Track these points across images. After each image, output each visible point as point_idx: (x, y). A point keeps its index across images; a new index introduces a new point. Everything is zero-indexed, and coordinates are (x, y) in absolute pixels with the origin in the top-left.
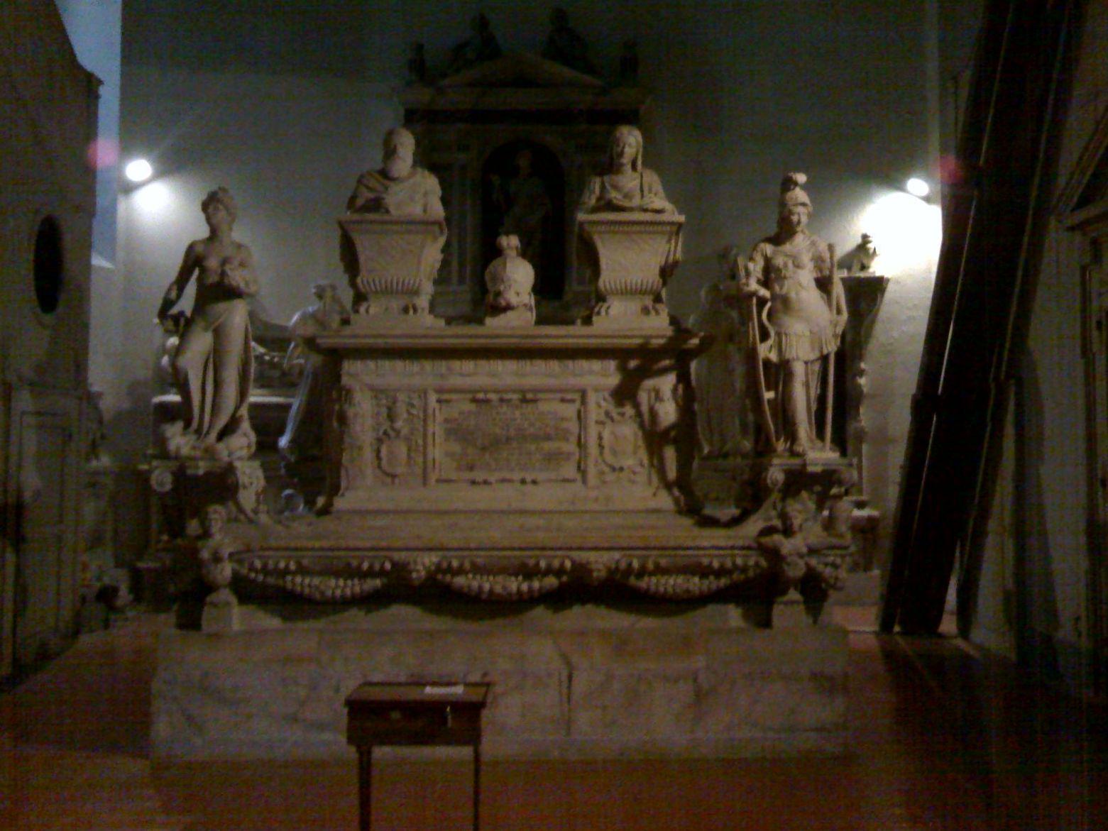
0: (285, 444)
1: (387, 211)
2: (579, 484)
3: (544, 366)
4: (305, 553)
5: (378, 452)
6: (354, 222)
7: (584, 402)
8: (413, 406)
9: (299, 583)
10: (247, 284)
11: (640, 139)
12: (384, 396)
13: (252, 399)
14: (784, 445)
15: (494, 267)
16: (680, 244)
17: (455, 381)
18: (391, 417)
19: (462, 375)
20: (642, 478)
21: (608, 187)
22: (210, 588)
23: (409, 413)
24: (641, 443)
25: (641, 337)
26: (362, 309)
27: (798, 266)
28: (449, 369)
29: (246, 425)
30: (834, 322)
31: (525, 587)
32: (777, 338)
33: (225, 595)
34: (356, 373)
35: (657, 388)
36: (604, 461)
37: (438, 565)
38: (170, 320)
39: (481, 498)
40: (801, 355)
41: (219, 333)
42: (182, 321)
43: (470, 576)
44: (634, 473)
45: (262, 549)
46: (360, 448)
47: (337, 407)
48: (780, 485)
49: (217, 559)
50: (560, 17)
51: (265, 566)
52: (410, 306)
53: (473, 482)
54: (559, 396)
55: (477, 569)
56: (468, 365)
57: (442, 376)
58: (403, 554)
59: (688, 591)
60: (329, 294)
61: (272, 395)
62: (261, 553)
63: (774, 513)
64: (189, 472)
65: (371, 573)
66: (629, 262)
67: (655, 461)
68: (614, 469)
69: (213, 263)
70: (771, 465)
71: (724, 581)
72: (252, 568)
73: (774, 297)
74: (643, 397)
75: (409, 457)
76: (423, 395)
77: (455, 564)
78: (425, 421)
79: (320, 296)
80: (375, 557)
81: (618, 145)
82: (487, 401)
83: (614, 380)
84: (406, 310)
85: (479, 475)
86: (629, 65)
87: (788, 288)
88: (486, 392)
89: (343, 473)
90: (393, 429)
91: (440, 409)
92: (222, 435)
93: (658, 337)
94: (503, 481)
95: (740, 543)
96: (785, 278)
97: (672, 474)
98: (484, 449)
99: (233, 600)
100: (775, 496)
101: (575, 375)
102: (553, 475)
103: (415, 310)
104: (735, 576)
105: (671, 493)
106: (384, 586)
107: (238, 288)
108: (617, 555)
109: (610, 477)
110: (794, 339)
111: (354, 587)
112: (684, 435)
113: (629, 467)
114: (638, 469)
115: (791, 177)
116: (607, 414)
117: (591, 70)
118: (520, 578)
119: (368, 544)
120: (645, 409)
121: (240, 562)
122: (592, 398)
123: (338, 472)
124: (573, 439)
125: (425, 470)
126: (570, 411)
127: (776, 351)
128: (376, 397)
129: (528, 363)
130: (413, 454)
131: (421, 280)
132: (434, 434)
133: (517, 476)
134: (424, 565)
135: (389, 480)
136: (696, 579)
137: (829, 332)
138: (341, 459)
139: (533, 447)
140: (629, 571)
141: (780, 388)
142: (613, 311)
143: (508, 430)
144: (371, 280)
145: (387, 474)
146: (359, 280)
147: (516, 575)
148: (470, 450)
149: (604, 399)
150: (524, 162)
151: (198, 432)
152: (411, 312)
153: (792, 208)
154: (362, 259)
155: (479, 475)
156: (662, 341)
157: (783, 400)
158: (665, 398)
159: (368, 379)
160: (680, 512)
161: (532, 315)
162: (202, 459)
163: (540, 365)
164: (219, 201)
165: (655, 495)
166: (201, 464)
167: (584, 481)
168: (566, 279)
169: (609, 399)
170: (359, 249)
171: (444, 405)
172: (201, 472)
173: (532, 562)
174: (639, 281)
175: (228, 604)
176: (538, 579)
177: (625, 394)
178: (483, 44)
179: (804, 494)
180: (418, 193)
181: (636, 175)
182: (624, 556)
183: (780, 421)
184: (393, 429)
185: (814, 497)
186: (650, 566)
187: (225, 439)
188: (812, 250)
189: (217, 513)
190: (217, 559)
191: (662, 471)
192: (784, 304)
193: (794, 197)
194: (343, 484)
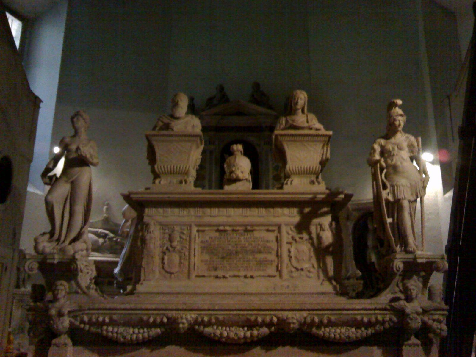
0: (117, 271)
1: (172, 129)
2: (278, 277)
4: (115, 312)
6: (154, 135)
7: (279, 231)
9: (110, 331)
10: (91, 156)
11: (306, 96)
14: (400, 249)
16: (329, 149)
17: (207, 220)
18: (171, 240)
22: (55, 334)
23: (181, 237)
24: (312, 254)
25: (310, 194)
27: (400, 148)
28: (203, 212)
31: (248, 334)
33: (65, 339)
34: (153, 215)
35: (321, 223)
36: (291, 264)
37: (196, 320)
39: (220, 285)
40: (406, 196)
41: (74, 185)
42: (54, 178)
43: (215, 327)
44: (309, 271)
45: (89, 309)
46: (152, 257)
47: (140, 234)
49: (60, 314)
50: (257, 86)
51: (90, 320)
53: (217, 277)
54: (266, 228)
55: (221, 323)
56: (215, 211)
57: (200, 217)
58: (174, 312)
59: (349, 337)
62: (88, 312)
63: (397, 289)
64: (49, 261)
65: (155, 325)
66: (303, 157)
67: (321, 265)
68: (297, 269)
70: (396, 259)
71: (370, 331)
72: (82, 322)
73: (388, 166)
74: (313, 229)
75: (181, 263)
76: (189, 228)
77: (206, 319)
78: (190, 242)
80: (158, 314)
82: (225, 231)
83: (297, 219)
84: (181, 182)
87: (396, 160)
88: (224, 226)
89: (142, 270)
90: (171, 246)
91: (199, 235)
93: (321, 194)
94: (234, 276)
95: (380, 306)
96: (393, 155)
97: (331, 273)
98: (223, 258)
99: (69, 341)
100: (398, 278)
101: (274, 216)
103: (186, 182)
104: (377, 328)
105: (331, 283)
106: (163, 333)
107: (86, 157)
108: (305, 314)
109: (295, 274)
110: (402, 188)
111: (144, 333)
112: (336, 250)
113: (306, 268)
114: (312, 270)
115: (394, 102)
116: (293, 238)
117: (270, 107)
118: (246, 329)
119: (154, 307)
120: (314, 235)
121: (75, 317)
122: (284, 229)
124: (274, 252)
126: (272, 236)
127: (392, 196)
129: (248, 209)
130: (182, 261)
131: (189, 167)
132: (195, 250)
133: (242, 273)
134: (186, 319)
135: (169, 275)
136: (353, 330)
139: (251, 257)
140: (312, 324)
143: (237, 247)
146: (156, 167)
147: (243, 327)
152: (184, 183)
153: (395, 117)
154: (158, 155)
155: (220, 273)
156: (323, 196)
157: (398, 223)
158: (326, 229)
159: (160, 219)
160: (337, 294)
161: (250, 185)
165: (322, 284)
167: (281, 276)
168: (269, 166)
170: (157, 150)
171: (200, 233)
172: (56, 261)
173: (253, 318)
175: (65, 344)
176: (256, 329)
177: (302, 227)
179: (415, 277)
182: (309, 314)
183: (397, 236)
184: (171, 246)
185: (421, 279)
186: (325, 321)
187: (73, 244)
188: (408, 140)
189: (63, 287)
190: (60, 314)
191: (325, 271)
194: (142, 277)
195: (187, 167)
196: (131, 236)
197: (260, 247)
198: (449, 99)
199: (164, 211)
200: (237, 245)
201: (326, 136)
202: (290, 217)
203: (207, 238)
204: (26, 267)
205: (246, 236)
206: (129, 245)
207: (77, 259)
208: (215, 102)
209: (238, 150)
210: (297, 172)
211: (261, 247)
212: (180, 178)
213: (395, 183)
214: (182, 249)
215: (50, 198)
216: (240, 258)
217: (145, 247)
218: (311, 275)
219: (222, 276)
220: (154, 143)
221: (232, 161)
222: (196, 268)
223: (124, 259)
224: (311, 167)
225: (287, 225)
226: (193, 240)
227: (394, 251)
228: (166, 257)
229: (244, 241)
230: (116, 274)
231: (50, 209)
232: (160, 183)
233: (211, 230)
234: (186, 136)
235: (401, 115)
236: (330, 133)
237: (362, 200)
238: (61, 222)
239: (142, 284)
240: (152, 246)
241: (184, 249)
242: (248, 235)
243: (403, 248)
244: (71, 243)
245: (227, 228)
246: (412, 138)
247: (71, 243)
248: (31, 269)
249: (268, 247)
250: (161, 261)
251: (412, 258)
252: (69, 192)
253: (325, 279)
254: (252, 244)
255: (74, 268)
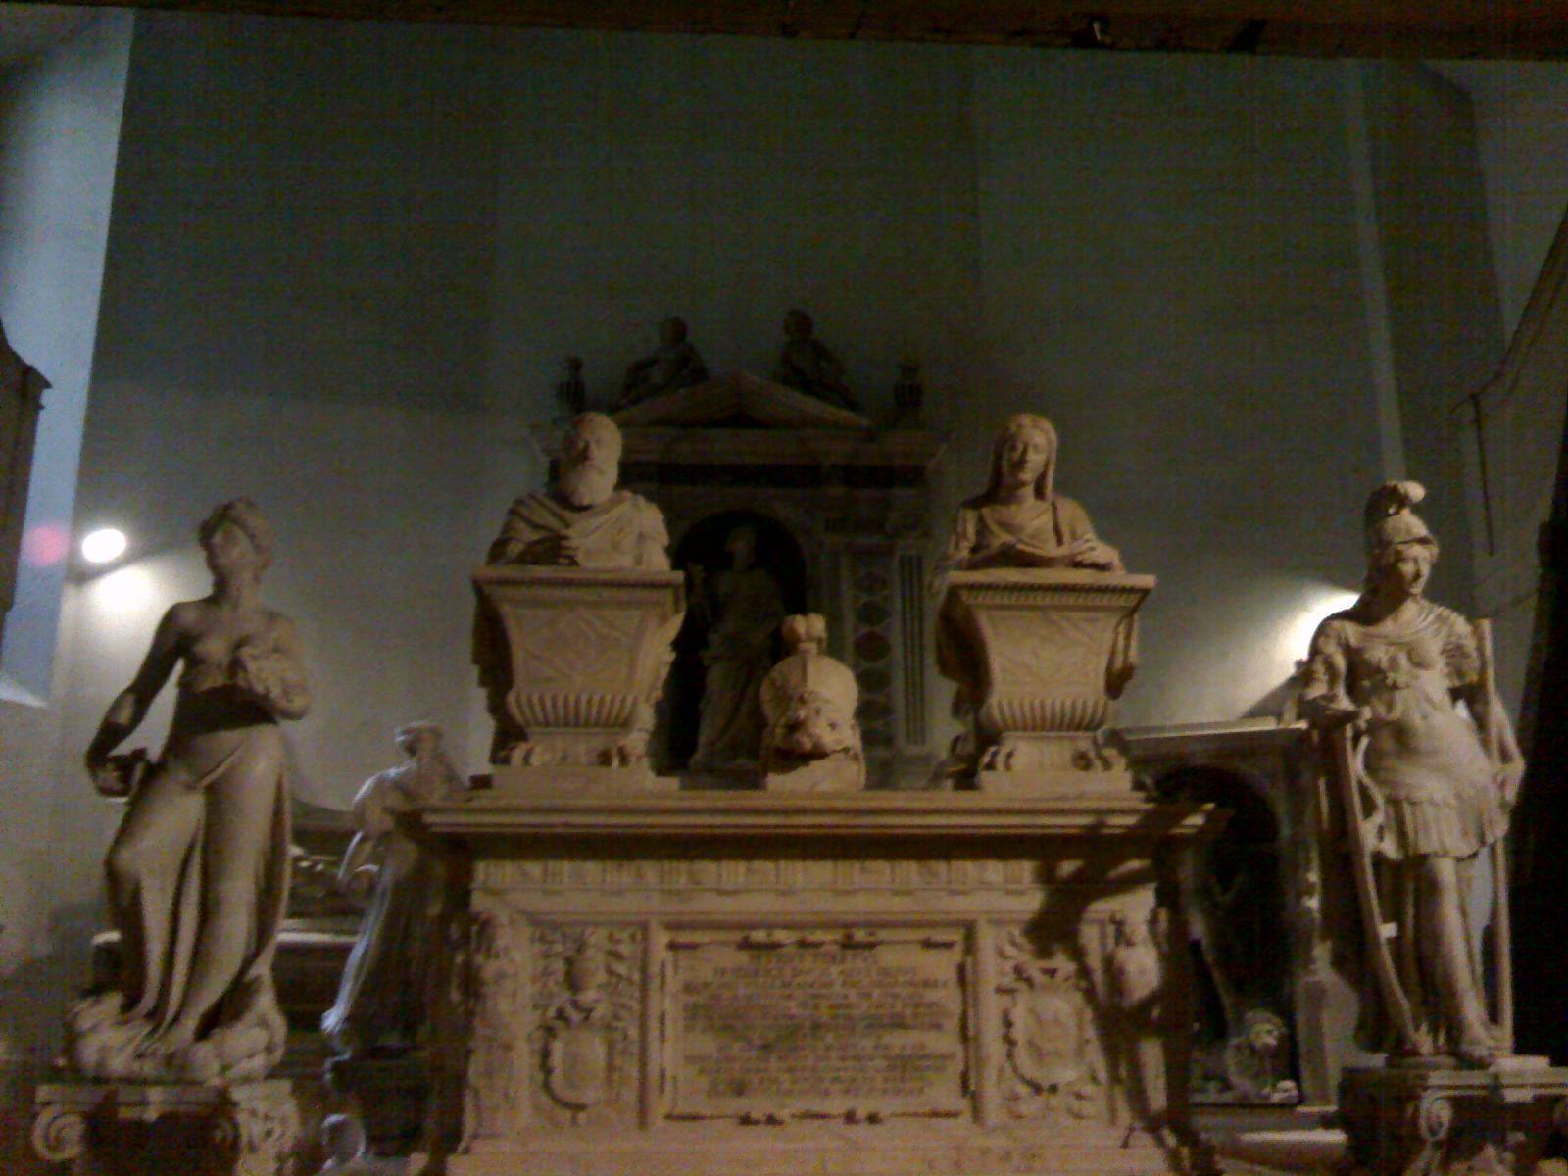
1: (573, 563)
2: (966, 1118)
3: (888, 872)
5: (546, 1054)
6: (503, 582)
7: (970, 946)
8: (617, 955)
10: (286, 692)
11: (1053, 436)
12: (558, 936)
13: (284, 937)
15: (781, 672)
18: (573, 981)
19: (721, 892)
20: (1094, 1107)
21: (994, 528)
23: (610, 972)
24: (1091, 1032)
26: (518, 755)
27: (1419, 663)
29: (265, 1002)
30: (1500, 778)
32: (1391, 810)
34: (505, 888)
35: (1118, 917)
36: (1015, 1069)
38: (110, 766)
41: (218, 799)
42: (138, 773)
44: (1079, 1096)
46: (507, 1047)
47: (459, 959)
48: (1442, 1134)
50: (800, 324)
52: (614, 751)
56: (734, 872)
60: (426, 748)
61: (309, 930)
64: (126, 1113)
67: (1123, 1072)
68: (1037, 1089)
69: (215, 648)
70: (1426, 1088)
74: (1090, 935)
75: (611, 1068)
78: (644, 988)
79: (411, 749)
81: (1013, 448)
82: (775, 946)
83: (1031, 901)
84: (605, 759)
85: (757, 1105)
86: (908, 398)
87: (1405, 706)
88: (770, 927)
89: (469, 1101)
90: (576, 1004)
92: (213, 1022)
93: (1123, 812)
96: (1395, 687)
97: (1158, 1098)
98: (766, 1047)
100: (1428, 1156)
101: (953, 893)
102: (913, 1104)
103: (624, 760)
105: (1161, 1142)
107: (266, 697)
109: (1030, 1106)
110: (1429, 812)
113: (1069, 1084)
114: (1089, 1089)
116: (1018, 971)
117: (851, 404)
120: (1094, 961)
122: (988, 939)
123: (459, 1096)
124: (952, 1025)
125: (642, 1100)
126: (942, 966)
128: (542, 939)
129: (857, 865)
130: (618, 1061)
132: (662, 1019)
133: (837, 1105)
135: (567, 1114)
137: (1493, 795)
138: (465, 1072)
139: (868, 1043)
141: (1410, 911)
142: (1018, 762)
143: (817, 1007)
144: (535, 698)
145: (566, 1105)
146: (511, 698)
148: (736, 1048)
149: (1014, 944)
150: (741, 545)
151: (155, 1015)
152: (616, 762)
153: (1401, 547)
154: (518, 656)
155: (757, 1105)
156: (1130, 821)
157: (1417, 942)
162: (158, 1082)
163: (881, 871)
164: (236, 522)
165: (1125, 1145)
166: (155, 1094)
167: (977, 1114)
169: (1020, 939)
171: (683, 954)
172: (151, 1115)
174: (1068, 703)
177: (1053, 930)
178: (681, 360)
179: (1490, 1151)
180: (628, 534)
181: (1045, 505)
184: (576, 1004)
187: (217, 1033)
188: (1445, 630)
192: (1399, 740)
193: (1403, 526)
195: (629, 702)
196: (384, 894)
197: (898, 1008)
198: (1477, 405)
199: (545, 871)
200: (816, 996)
201: (1132, 590)
202: (1009, 893)
203: (706, 974)
204: (39, 1145)
205: (848, 965)
206: (379, 925)
207: (235, 1104)
208: (657, 376)
209: (810, 638)
210: (1029, 722)
211: (905, 1006)
212: (598, 743)
213: (1403, 793)
214: (617, 1017)
215: (126, 858)
216: (828, 1048)
217: (479, 1009)
218: (1088, 1108)
219: (764, 1119)
220: (505, 609)
221: (794, 679)
222: (669, 1088)
223: (361, 980)
224: (1079, 705)
225: (998, 922)
226: (655, 984)
227: (1409, 1046)
228: (558, 1048)
229: (844, 984)
230: (330, 1035)
231: (125, 901)
232: (526, 759)
233: (723, 943)
234: (621, 585)
235: (1423, 541)
236: (1147, 580)
237: (1162, 729)
238: (167, 945)
239: (467, 1151)
240: (503, 1006)
241: (624, 1014)
242: (855, 962)
243: (1441, 1039)
244: (205, 1031)
245: (781, 935)
246: (1460, 625)
247: (205, 1031)
248: (56, 1144)
249: (931, 1005)
250: (537, 1060)
251: (1484, 1087)
252: (198, 829)
253: (1138, 1124)
254: (868, 995)
255: (225, 1138)
